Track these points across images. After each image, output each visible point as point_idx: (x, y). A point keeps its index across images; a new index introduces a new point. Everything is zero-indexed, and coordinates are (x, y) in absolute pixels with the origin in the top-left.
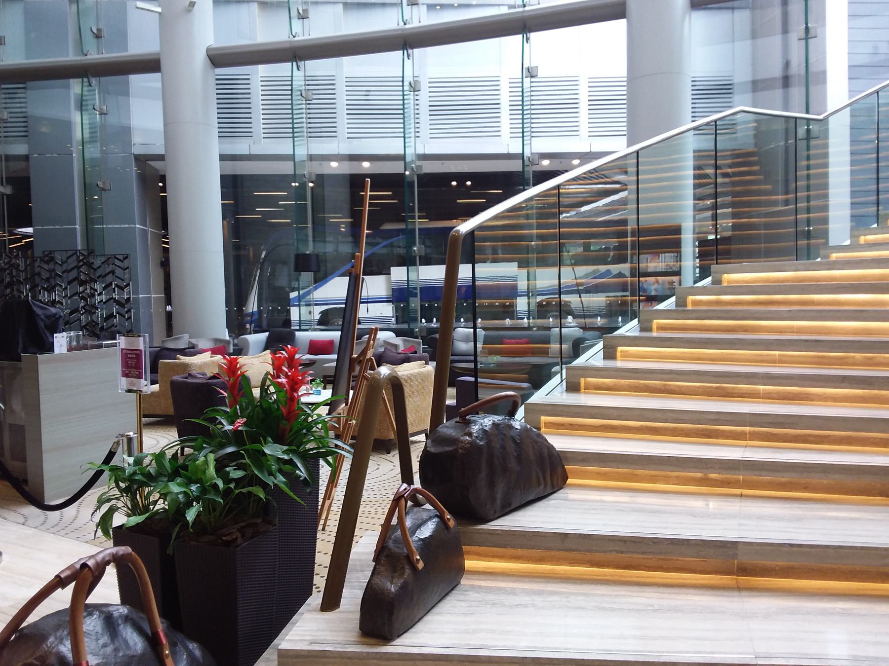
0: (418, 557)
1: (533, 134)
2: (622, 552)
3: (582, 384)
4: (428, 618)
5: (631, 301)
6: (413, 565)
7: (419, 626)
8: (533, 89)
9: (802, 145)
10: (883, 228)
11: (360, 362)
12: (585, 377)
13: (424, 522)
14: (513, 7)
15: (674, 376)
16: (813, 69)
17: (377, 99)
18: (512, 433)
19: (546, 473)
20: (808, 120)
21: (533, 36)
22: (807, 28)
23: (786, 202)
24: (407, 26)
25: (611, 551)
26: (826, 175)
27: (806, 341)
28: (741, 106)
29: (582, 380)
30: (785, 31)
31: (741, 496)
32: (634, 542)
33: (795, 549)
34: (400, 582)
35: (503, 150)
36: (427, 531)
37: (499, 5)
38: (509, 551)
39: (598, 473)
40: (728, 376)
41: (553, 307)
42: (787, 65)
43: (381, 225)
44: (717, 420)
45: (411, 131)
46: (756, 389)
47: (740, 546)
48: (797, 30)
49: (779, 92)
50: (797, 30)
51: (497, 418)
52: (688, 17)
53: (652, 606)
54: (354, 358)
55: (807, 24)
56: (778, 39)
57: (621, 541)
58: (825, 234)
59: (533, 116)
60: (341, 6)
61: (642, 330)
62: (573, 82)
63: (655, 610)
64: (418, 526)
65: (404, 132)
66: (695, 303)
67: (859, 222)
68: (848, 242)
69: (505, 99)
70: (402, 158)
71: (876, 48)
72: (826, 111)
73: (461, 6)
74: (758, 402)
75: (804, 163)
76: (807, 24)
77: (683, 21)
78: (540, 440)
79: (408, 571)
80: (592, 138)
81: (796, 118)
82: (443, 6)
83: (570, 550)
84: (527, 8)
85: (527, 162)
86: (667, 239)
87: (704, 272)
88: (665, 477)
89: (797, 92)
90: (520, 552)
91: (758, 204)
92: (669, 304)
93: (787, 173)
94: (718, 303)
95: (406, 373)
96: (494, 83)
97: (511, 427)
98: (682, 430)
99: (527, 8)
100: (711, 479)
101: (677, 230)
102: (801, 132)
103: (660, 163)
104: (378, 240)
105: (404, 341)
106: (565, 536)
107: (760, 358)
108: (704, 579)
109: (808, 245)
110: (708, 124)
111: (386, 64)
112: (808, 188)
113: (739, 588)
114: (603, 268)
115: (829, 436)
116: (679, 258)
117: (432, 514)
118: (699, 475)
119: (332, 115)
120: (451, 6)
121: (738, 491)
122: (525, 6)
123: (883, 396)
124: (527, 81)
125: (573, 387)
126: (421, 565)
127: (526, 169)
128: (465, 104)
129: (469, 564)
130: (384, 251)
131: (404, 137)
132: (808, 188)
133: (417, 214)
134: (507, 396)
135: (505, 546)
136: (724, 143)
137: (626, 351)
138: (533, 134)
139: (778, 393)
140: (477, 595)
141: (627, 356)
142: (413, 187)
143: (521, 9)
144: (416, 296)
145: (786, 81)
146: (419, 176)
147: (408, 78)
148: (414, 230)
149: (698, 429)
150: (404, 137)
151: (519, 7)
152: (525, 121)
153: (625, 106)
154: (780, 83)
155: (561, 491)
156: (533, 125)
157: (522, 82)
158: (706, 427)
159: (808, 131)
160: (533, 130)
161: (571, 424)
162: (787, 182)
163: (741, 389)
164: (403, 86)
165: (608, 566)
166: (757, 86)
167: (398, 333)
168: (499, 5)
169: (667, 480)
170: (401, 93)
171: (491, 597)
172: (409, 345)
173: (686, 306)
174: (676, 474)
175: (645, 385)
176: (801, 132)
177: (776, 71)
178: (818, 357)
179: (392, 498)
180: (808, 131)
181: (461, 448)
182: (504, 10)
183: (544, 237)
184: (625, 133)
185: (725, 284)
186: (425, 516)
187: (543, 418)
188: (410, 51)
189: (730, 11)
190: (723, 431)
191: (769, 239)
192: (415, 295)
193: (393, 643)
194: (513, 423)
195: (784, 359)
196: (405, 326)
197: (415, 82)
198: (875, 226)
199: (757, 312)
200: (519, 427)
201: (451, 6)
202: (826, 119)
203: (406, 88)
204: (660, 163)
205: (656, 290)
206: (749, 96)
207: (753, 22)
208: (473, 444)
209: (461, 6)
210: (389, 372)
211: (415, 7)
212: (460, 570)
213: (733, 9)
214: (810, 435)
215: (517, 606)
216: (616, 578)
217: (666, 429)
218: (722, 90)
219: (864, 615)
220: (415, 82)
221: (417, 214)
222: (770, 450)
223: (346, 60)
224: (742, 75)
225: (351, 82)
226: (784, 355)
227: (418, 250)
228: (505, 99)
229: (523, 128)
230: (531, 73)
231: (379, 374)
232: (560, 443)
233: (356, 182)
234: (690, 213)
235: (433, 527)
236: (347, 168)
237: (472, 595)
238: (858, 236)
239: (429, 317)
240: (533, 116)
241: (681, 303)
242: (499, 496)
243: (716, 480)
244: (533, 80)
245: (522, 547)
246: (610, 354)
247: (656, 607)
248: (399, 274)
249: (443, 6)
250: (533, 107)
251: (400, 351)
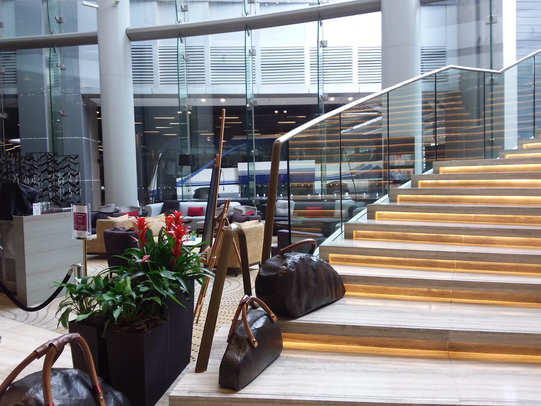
0: (254, 340)
1: (324, 82)
2: (379, 337)
3: (354, 234)
4: (261, 377)
5: (384, 183)
6: (251, 345)
7: (255, 382)
8: (324, 54)
9: (488, 88)
10: (537, 139)
11: (219, 221)
12: (356, 230)
13: (258, 318)
14: (312, 4)
15: (410, 229)
16: (495, 42)
17: (229, 60)
18: (312, 264)
19: (332, 288)
20: (492, 73)
21: (324, 22)
22: (491, 17)
24: (248, 16)
25: (372, 336)
26: (503, 107)
27: (491, 208)
28: (451, 64)
29: (354, 232)
30: (478, 19)
31: (451, 302)
32: (386, 330)
33: (484, 335)
34: (243, 355)
35: (306, 92)
36: (260, 324)
37: (304, 3)
38: (310, 336)
39: (364, 288)
40: (443, 230)
41: (336, 187)
42: (479, 40)
43: (232, 137)
44: (436, 256)
45: (250, 80)
46: (460, 237)
47: (450, 333)
48: (485, 18)
49: (474, 56)
50: (485, 18)
51: (302, 255)
52: (418, 10)
53: (397, 369)
54: (215, 218)
55: (491, 15)
56: (473, 24)
57: (378, 330)
58: (502, 143)
59: (324, 71)
60: (207, 4)
61: (391, 201)
62: (349, 50)
63: (399, 372)
64: (254, 321)
65: (246, 81)
66: (423, 185)
67: (522, 135)
68: (516, 148)
69: (307, 60)
70: (245, 96)
71: (533, 29)
72: (502, 68)
73: (280, 4)
74: (461, 245)
75: (490, 99)
76: (491, 15)
77: (416, 13)
78: (328, 268)
80: (360, 84)
81: (484, 72)
82: (270, 4)
83: (347, 335)
84: (321, 5)
85: (320, 99)
86: (406, 146)
87: (429, 166)
88: (405, 291)
89: (485, 56)
90: (316, 336)
91: (461, 124)
92: (407, 185)
93: (479, 105)
94: (437, 185)
95: (247, 227)
96: (300, 51)
97: (311, 260)
98: (415, 262)
99: (321, 5)
100: (433, 292)
101: (412, 140)
102: (488, 80)
103: (401, 99)
104: (230, 146)
105: (246, 208)
106: (344, 327)
107: (463, 218)
108: (429, 353)
109: (492, 149)
110: (431, 76)
111: (235, 39)
112: (492, 115)
113: (450, 359)
114: (367, 163)
115: (505, 266)
116: (413, 158)
117: (263, 314)
118: (425, 289)
119: (202, 70)
120: (274, 4)
121: (449, 299)
122: (319, 4)
123: (537, 241)
124: (321, 49)
125: (348, 236)
126: (256, 345)
127: (320, 103)
128: (283, 64)
129: (285, 344)
130: (234, 153)
131: (246, 84)
132: (492, 115)
133: (254, 130)
134: (308, 242)
135: (307, 333)
136: (441, 87)
137: (381, 214)
138: (324, 82)
139: (474, 239)
140: (290, 363)
141: (381, 217)
142: (252, 114)
143: (317, 6)
144: (253, 181)
145: (478, 49)
146: (255, 107)
147: (248, 48)
148: (252, 140)
149: (425, 262)
150: (246, 84)
151: (316, 4)
152: (320, 74)
153: (380, 65)
154: (475, 50)
155: (341, 299)
156: (324, 76)
157: (318, 50)
158: (430, 260)
159: (492, 80)
160: (324, 79)
161: (347, 259)
162: (479, 111)
163: (451, 237)
164: (245, 52)
165: (370, 345)
166: (461, 52)
167: (242, 203)
168: (304, 3)
169: (406, 293)
170: (244, 57)
171: (299, 364)
172: (249, 210)
173: (417, 186)
174: (411, 289)
175: (392, 235)
176: (488, 80)
177: (473, 43)
178: (498, 218)
179: (238, 303)
180: (492, 80)
181: (280, 273)
182: (307, 6)
183: (331, 145)
184: (380, 81)
185: (441, 173)
186: (259, 314)
187: (330, 255)
188: (250, 31)
189: (445, 7)
190: (440, 263)
191: (468, 146)
192: (253, 180)
193: (239, 392)
194: (312, 258)
195: (477, 219)
196: (247, 199)
197: (253, 50)
198: (533, 138)
199: (460, 190)
200: (316, 261)
201: (274, 4)
202: (503, 73)
203: (247, 54)
204: (401, 99)
205: (399, 177)
206: (456, 59)
207: (458, 14)
208: (288, 271)
209: (280, 4)
210: (237, 227)
211: (252, 4)
212: (280, 348)
213: (446, 5)
214: (493, 265)
215: (314, 369)
216: (375, 352)
217: (405, 261)
218: (439, 55)
219: (526, 375)
220: (253, 50)
221: (254, 130)
222: (468, 274)
223: (211, 36)
224: (451, 46)
225: (214, 50)
226: (477, 217)
227: (255, 152)
228: (307, 60)
229: (318, 78)
230: (323, 44)
231: (231, 228)
232: (341, 270)
233: (217, 111)
234: (420, 130)
236: (211, 103)
237: (288, 363)
238: (522, 144)
239: (261, 193)
240: (324, 71)
241: (415, 185)
242: (304, 302)
243: (435, 293)
244: (324, 49)
245: (318, 333)
246: (371, 216)
247: (399, 370)
248: (243, 167)
249: (270, 4)
250: (324, 65)
251: (243, 214)
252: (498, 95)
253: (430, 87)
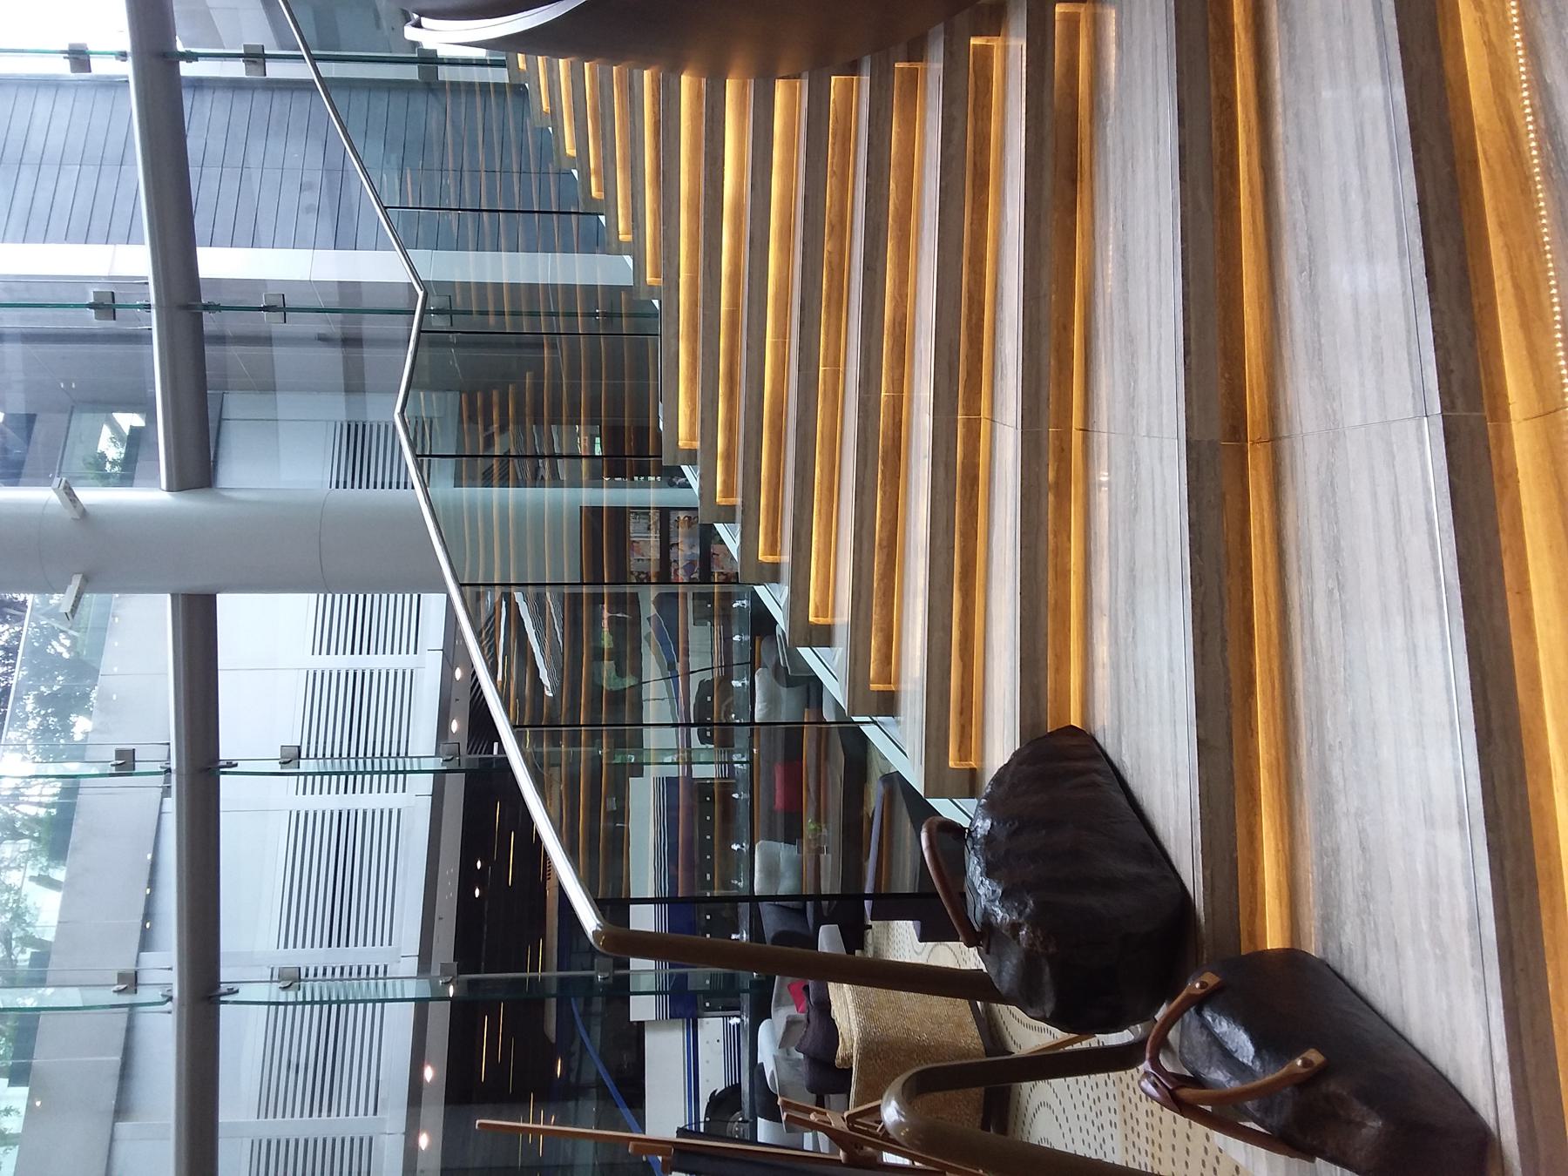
0: (1299, 1062)
1: (402, 754)
2: (1224, 640)
3: (881, 687)
4: (1417, 1036)
5: (717, 588)
6: (1314, 1077)
7: (1441, 1059)
8: (320, 755)
9: (461, 323)
10: (607, 207)
11: (859, 1144)
12: (867, 681)
13: (1217, 1042)
14: (166, 792)
15: (865, 533)
16: (334, 302)
17: (304, 1052)
18: (1002, 835)
19: (1065, 772)
20: (424, 311)
21: (224, 754)
22: (265, 309)
23: (553, 346)
24: (175, 994)
25: (1224, 661)
26: (514, 287)
27: (802, 324)
28: (390, 410)
29: (874, 687)
30: (267, 340)
31: (1085, 430)
32: (1203, 617)
33: (1193, 347)
34: (1359, 1109)
35: (427, 802)
36: (1242, 1044)
37: (160, 813)
38: (1241, 854)
39: (1057, 670)
40: (866, 447)
41: (711, 720)
42: (324, 339)
43: (546, 1038)
44: (946, 465)
45: (371, 989)
47: (1196, 437)
48: (271, 323)
49: (368, 353)
50: (271, 323)
51: (974, 868)
52: (226, 493)
53: (1331, 592)
54: (848, 1157)
55: (260, 309)
56: (278, 352)
57: (1203, 641)
58: (613, 291)
59: (369, 754)
60: (123, 1128)
61: (775, 578)
62: (315, 679)
63: (1341, 587)
64: (1228, 1057)
65: (374, 1001)
66: (729, 490)
67: (597, 242)
68: (629, 260)
69: (331, 801)
70: (421, 1004)
71: (308, 210)
72: (411, 284)
73: (152, 882)
74: (911, 400)
75: (492, 319)
76: (260, 309)
77: (230, 500)
78: (1007, 778)
79: (1333, 1086)
80: (417, 653)
81: (420, 331)
82: (148, 915)
83: (1230, 735)
84: (173, 766)
85: (453, 765)
86: (605, 532)
87: (672, 476)
88: (1056, 555)
89: (371, 327)
90: (1241, 831)
91: (556, 388)
92: (730, 537)
93: (508, 345)
94: (729, 455)
95: (853, 1017)
96: (301, 822)
97: (990, 837)
98: (964, 522)
99: (173, 766)
100: (1057, 477)
101: (595, 512)
102: (438, 322)
103: (474, 541)
104: (576, 1047)
105: (779, 1004)
106: (1202, 744)
107: (830, 394)
108: (1259, 496)
109: (629, 316)
110: (419, 468)
111: (243, 1035)
112: (534, 314)
113: (1274, 439)
114: (647, 629)
115: (969, 291)
116: (643, 511)
117: (1195, 1023)
118: (1051, 498)
119: (330, 1146)
120: (150, 902)
121: (1076, 437)
122: (169, 770)
123: (896, 209)
124: (306, 765)
125: (888, 704)
126: (1315, 1057)
127: (463, 767)
128: (334, 877)
129: (1274, 938)
130: (597, 1030)
131: (383, 1001)
132: (534, 314)
133: (528, 974)
134: (931, 846)
135: (1234, 862)
136: (445, 443)
137: (817, 607)
138: (402, 754)
139: (892, 368)
140: (1348, 928)
141: (826, 606)
142: (477, 981)
143: (174, 777)
144: (685, 976)
145: (351, 342)
146: (460, 972)
147: (274, 992)
148: (561, 980)
149: (963, 497)
150: (383, 1001)
151: (167, 781)
152: (377, 768)
153: (369, 596)
154: (353, 351)
155: (1100, 740)
156: (386, 754)
157: (306, 774)
158: (959, 487)
159: (438, 312)
160: (394, 754)
161: (961, 713)
162: (528, 345)
163: (886, 426)
164: (286, 1004)
165: (1251, 665)
166: (354, 385)
167: (761, 1012)
168: (160, 813)
169: (1063, 552)
170: (299, 1007)
171: (1349, 898)
172: (787, 995)
173: (733, 507)
174: (1051, 537)
175: (881, 580)
176: (438, 322)
177: (335, 354)
178: (828, 306)
179: (1168, 1114)
180: (438, 312)
181: (1046, 948)
182: (171, 804)
184: (415, 596)
185: (697, 445)
186: (1198, 1037)
187: (951, 764)
188: (224, 988)
189: (224, 423)
190: (965, 456)
191: (616, 372)
192: (683, 978)
193: (1491, 1123)
194: (980, 833)
195: (831, 359)
196: (746, 1000)
197: (281, 978)
198: (602, 218)
199: (748, 397)
200: (988, 823)
201: (150, 902)
202: (424, 285)
203: (291, 999)
204: (474, 541)
205: (691, 547)
206: (370, 398)
207: (245, 388)
208: (1035, 921)
209: (152, 882)
210: (894, 1103)
211: (143, 978)
212: (1293, 958)
213: (220, 420)
214: (969, 321)
215: (1363, 849)
216: (1274, 651)
217: (964, 550)
218: (357, 444)
219: (1310, 238)
220: (281, 978)
221: (528, 974)
222: (998, 383)
223: (224, 1117)
224: (336, 408)
225: (268, 1104)
226: (826, 358)
227: (603, 971)
228: (331, 801)
229: (388, 772)
230: (291, 758)
232: (1001, 745)
233: (463, 1090)
234: (565, 494)
235: (1224, 1023)
236: (434, 1112)
237: (1350, 934)
238: (619, 243)
239: (723, 953)
240: (369, 754)
241: (728, 515)
242: (1133, 868)
243: (1058, 472)
244: (303, 755)
245: (1232, 828)
246: (822, 636)
247: (1332, 584)
248: (642, 1008)
249: (148, 915)
250: (353, 754)
251: (803, 1016)
252: (482, 297)
253: (444, 472)
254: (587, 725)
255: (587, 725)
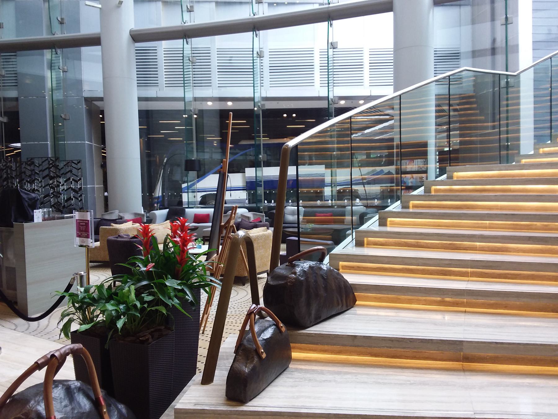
0: (262, 351)
1: (335, 85)
2: (390, 347)
3: (365, 242)
4: (269, 389)
5: (396, 189)
6: (259, 356)
7: (263, 394)
8: (334, 56)
9: (503, 91)
10: (554, 143)
11: (226, 228)
12: (367, 237)
13: (266, 329)
14: (322, 4)
15: (423, 236)
16: (510, 43)
17: (236, 62)
18: (321, 272)
19: (343, 297)
20: (507, 75)
21: (335, 22)
22: (506, 18)
24: (256, 17)
25: (384, 347)
26: (518, 110)
27: (506, 214)
28: (465, 66)
29: (365, 239)
30: (493, 19)
31: (465, 312)
32: (398, 341)
33: (499, 345)
34: (251, 366)
35: (316, 94)
36: (268, 334)
37: (313, 3)
38: (320, 347)
39: (375, 298)
40: (457, 237)
41: (347, 193)
42: (494, 41)
43: (239, 141)
44: (450, 264)
45: (258, 82)
47: (464, 344)
48: (500, 19)
49: (489, 58)
50: (500, 19)
51: (312, 263)
52: (432, 10)
53: (409, 381)
54: (222, 225)
55: (506, 15)
56: (488, 25)
57: (390, 340)
58: (518, 147)
59: (334, 73)
60: (214, 4)
61: (403, 207)
62: (360, 51)
63: (411, 384)
64: (262, 331)
65: (254, 83)
66: (436, 191)
67: (539, 140)
68: (532, 153)
69: (317, 62)
70: (253, 99)
71: (550, 30)
72: (518, 70)
73: (289, 4)
74: (476, 253)
75: (505, 103)
76: (506, 15)
77: (429, 13)
78: (339, 277)
80: (372, 87)
81: (500, 74)
82: (278, 4)
83: (358, 346)
84: (331, 5)
85: (330, 102)
86: (419, 150)
87: (442, 171)
88: (417, 300)
89: (500, 58)
90: (326, 347)
91: (476, 128)
92: (420, 191)
93: (494, 109)
94: (451, 190)
95: (255, 234)
96: (310, 52)
97: (321, 269)
98: (428, 270)
99: (331, 5)
100: (447, 302)
101: (425, 145)
102: (503, 83)
103: (414, 102)
104: (237, 151)
105: (254, 214)
106: (355, 337)
107: (477, 225)
108: (442, 364)
109: (507, 154)
110: (444, 78)
111: (242, 40)
112: (507, 118)
113: (464, 370)
114: (378, 169)
115: (520, 274)
116: (426, 163)
117: (271, 324)
118: (439, 299)
119: (208, 73)
120: (283, 4)
121: (463, 309)
122: (329, 4)
123: (554, 249)
124: (331, 51)
125: (359, 244)
126: (264, 356)
127: (330, 106)
128: (292, 66)
129: (294, 355)
130: (241, 158)
131: (254, 86)
132: (507, 118)
133: (262, 135)
134: (318, 249)
135: (317, 344)
136: (454, 90)
137: (393, 221)
138: (335, 85)
139: (488, 247)
140: (299, 374)
141: (393, 224)
142: (260, 118)
143: (327, 6)
144: (261, 186)
145: (493, 51)
146: (263, 111)
147: (256, 49)
148: (260, 145)
149: (438, 270)
150: (254, 86)
151: (326, 4)
152: (330, 76)
153: (392, 67)
154: (490, 52)
155: (352, 309)
156: (334, 79)
157: (328, 52)
158: (443, 269)
159: (507, 82)
160: (334, 82)
161: (358, 267)
162: (494, 114)
163: (465, 245)
164: (253, 54)
165: (381, 356)
166: (475, 54)
167: (250, 210)
168: (313, 3)
169: (418, 302)
170: (252, 59)
171: (308, 376)
172: (257, 217)
173: (430, 192)
174: (424, 298)
175: (405, 242)
176: (503, 83)
177: (487, 45)
178: (514, 224)
179: (246, 313)
180: (507, 82)
181: (289, 282)
182: (316, 6)
184: (392, 84)
185: (455, 179)
186: (267, 324)
187: (341, 263)
188: (257, 32)
189: (458, 7)
190: (454, 271)
191: (483, 150)
192: (261, 186)
193: (247, 405)
194: (322, 266)
195: (492, 226)
196: (254, 205)
197: (261, 51)
198: (549, 142)
199: (475, 196)
200: (326, 269)
201: (283, 4)
202: (518, 75)
203: (255, 55)
204: (414, 102)
205: (412, 182)
206: (470, 61)
207: (473, 14)
208: (297, 279)
209: (289, 4)
210: (244, 234)
211: (260, 5)
212: (289, 359)
213: (460, 5)
214: (508, 274)
215: (324, 381)
216: (387, 364)
217: (418, 270)
218: (453, 57)
219: (542, 387)
220: (261, 51)
221: (262, 135)
222: (483, 283)
223: (217, 38)
224: (466, 47)
225: (220, 51)
226: (492, 224)
227: (263, 157)
228: (317, 62)
229: (328, 80)
230: (333, 46)
232: (351, 278)
233: (223, 114)
234: (433, 134)
236: (218, 106)
237: (297, 374)
238: (539, 149)
239: (269, 199)
240: (334, 73)
241: (428, 191)
242: (313, 312)
243: (449, 302)
244: (334, 50)
245: (328, 344)
246: (383, 223)
247: (412, 382)
248: (250, 172)
249: (278, 4)
250: (334, 67)
251: (251, 221)
254: (341, 149)
255: (341, 149)
